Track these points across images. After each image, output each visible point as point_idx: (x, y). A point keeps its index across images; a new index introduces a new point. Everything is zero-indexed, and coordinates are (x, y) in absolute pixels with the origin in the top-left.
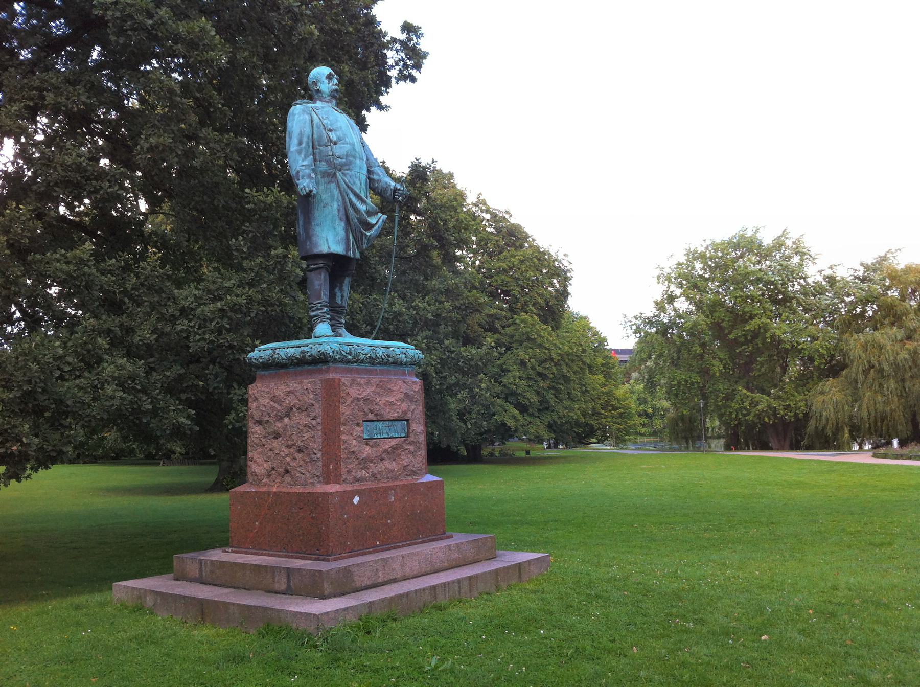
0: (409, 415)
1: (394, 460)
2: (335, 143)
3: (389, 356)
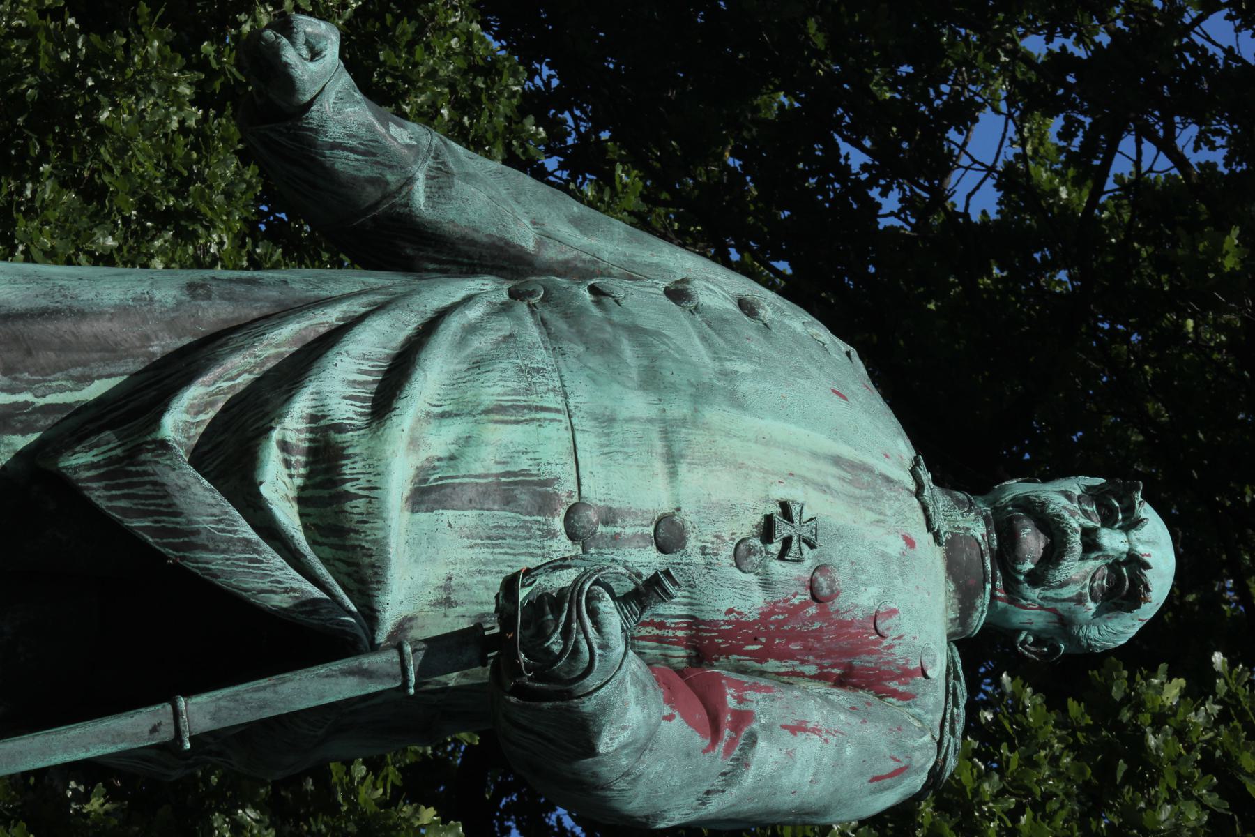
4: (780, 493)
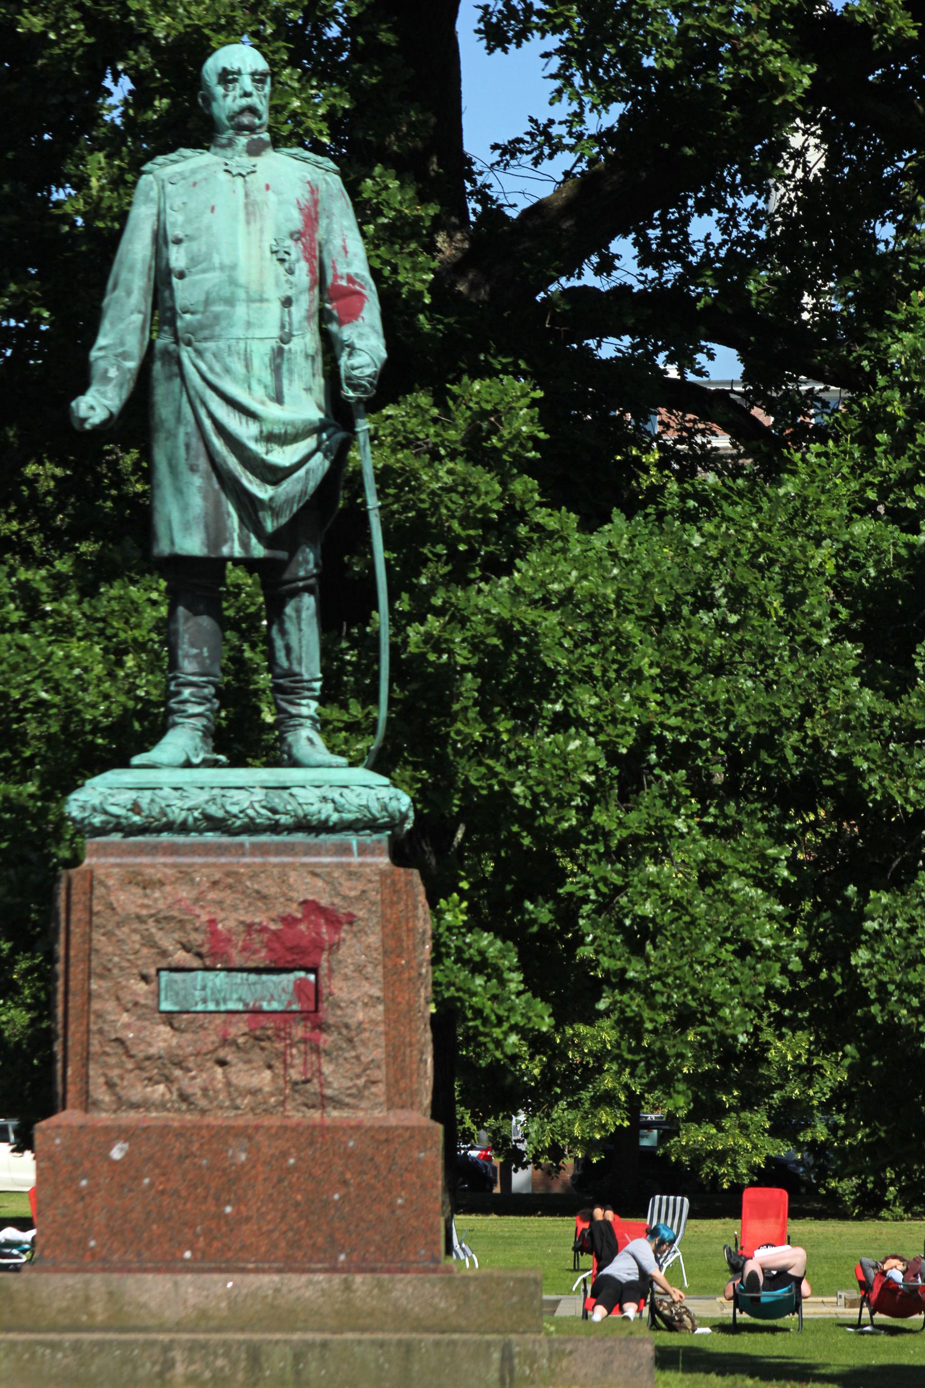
3: (274, 811)
4: (268, 254)
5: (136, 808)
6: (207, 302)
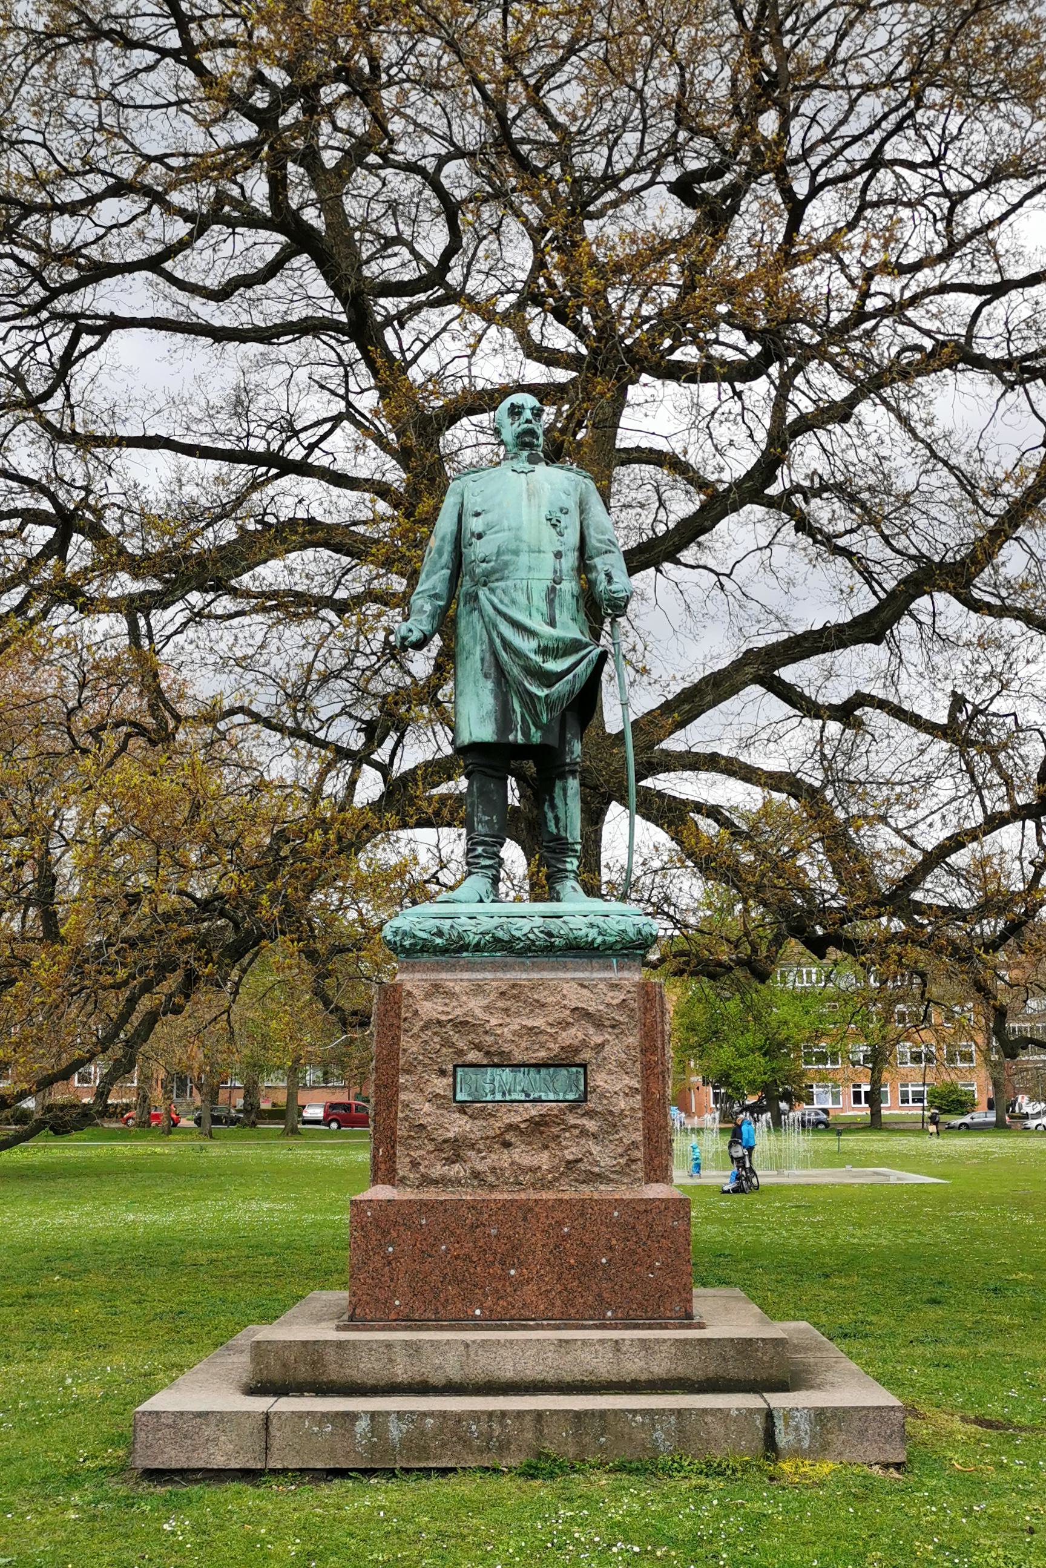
0: (586, 1055)
1: (547, 1147)
2: (480, 536)
3: (550, 934)
5: (440, 933)
6: (498, 554)
